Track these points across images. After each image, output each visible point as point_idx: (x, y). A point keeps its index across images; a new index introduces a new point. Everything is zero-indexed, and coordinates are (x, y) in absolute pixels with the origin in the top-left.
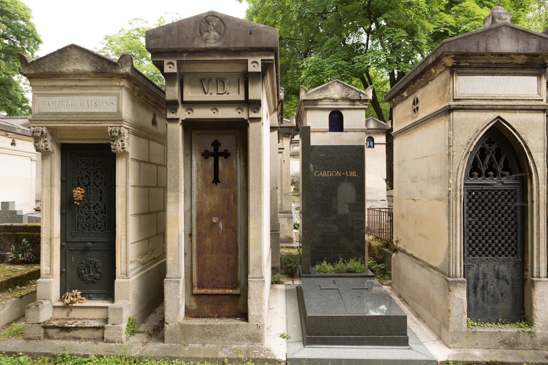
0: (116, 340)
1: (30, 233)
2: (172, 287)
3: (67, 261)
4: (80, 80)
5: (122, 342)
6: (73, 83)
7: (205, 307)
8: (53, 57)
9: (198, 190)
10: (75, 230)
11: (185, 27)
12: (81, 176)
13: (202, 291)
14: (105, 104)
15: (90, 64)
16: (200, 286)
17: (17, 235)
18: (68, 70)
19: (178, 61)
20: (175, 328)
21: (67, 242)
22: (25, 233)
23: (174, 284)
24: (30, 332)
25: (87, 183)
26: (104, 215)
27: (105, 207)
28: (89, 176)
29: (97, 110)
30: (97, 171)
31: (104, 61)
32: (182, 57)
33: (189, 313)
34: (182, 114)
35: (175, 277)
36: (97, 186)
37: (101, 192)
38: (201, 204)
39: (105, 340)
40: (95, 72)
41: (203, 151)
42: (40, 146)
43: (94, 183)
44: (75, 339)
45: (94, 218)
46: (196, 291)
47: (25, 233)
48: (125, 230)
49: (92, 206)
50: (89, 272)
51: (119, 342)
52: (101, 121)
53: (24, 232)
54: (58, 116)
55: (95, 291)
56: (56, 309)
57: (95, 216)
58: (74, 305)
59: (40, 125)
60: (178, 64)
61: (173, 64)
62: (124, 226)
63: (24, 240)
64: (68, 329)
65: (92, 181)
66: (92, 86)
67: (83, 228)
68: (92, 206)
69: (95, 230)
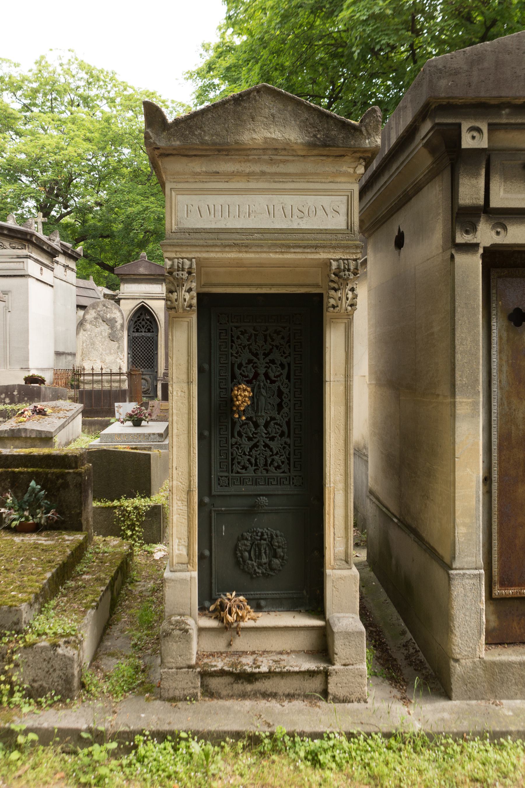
0: (353, 697)
1: (41, 470)
2: (468, 587)
3: (213, 534)
4: (272, 162)
5: (365, 702)
6: (257, 168)
7: (515, 624)
8: (221, 112)
9: (501, 388)
10: (227, 471)
11: (510, 53)
12: (239, 360)
13: (511, 592)
14: (320, 212)
15: (300, 127)
16: (503, 584)
17: (13, 472)
18: (253, 139)
19: (489, 125)
20: (474, 669)
21: (210, 495)
22: (30, 470)
23: (471, 582)
24: (174, 685)
25: (251, 376)
26: (288, 440)
27: (288, 423)
28: (255, 360)
29: (304, 225)
30: (271, 351)
31: (332, 122)
32: (500, 116)
33: (496, 638)
34: (486, 235)
35: (470, 566)
36: (273, 382)
37: (280, 393)
38: (508, 418)
39: (330, 697)
40: (311, 145)
41: (511, 311)
42: (181, 300)
43: (266, 375)
44: (266, 695)
45: (266, 446)
46: (497, 592)
47: (30, 470)
48: (342, 471)
49: (262, 422)
50: (259, 556)
51: (359, 701)
52: (316, 247)
53: (26, 467)
54: (221, 236)
55: (270, 593)
56: (203, 633)
57: (267, 441)
58: (242, 624)
59: (184, 255)
60: (490, 131)
61: (479, 130)
62: (342, 462)
63: (33, 483)
64: (251, 677)
65: (262, 371)
66: (296, 174)
67: (244, 468)
68: (262, 422)
69: (267, 471)
